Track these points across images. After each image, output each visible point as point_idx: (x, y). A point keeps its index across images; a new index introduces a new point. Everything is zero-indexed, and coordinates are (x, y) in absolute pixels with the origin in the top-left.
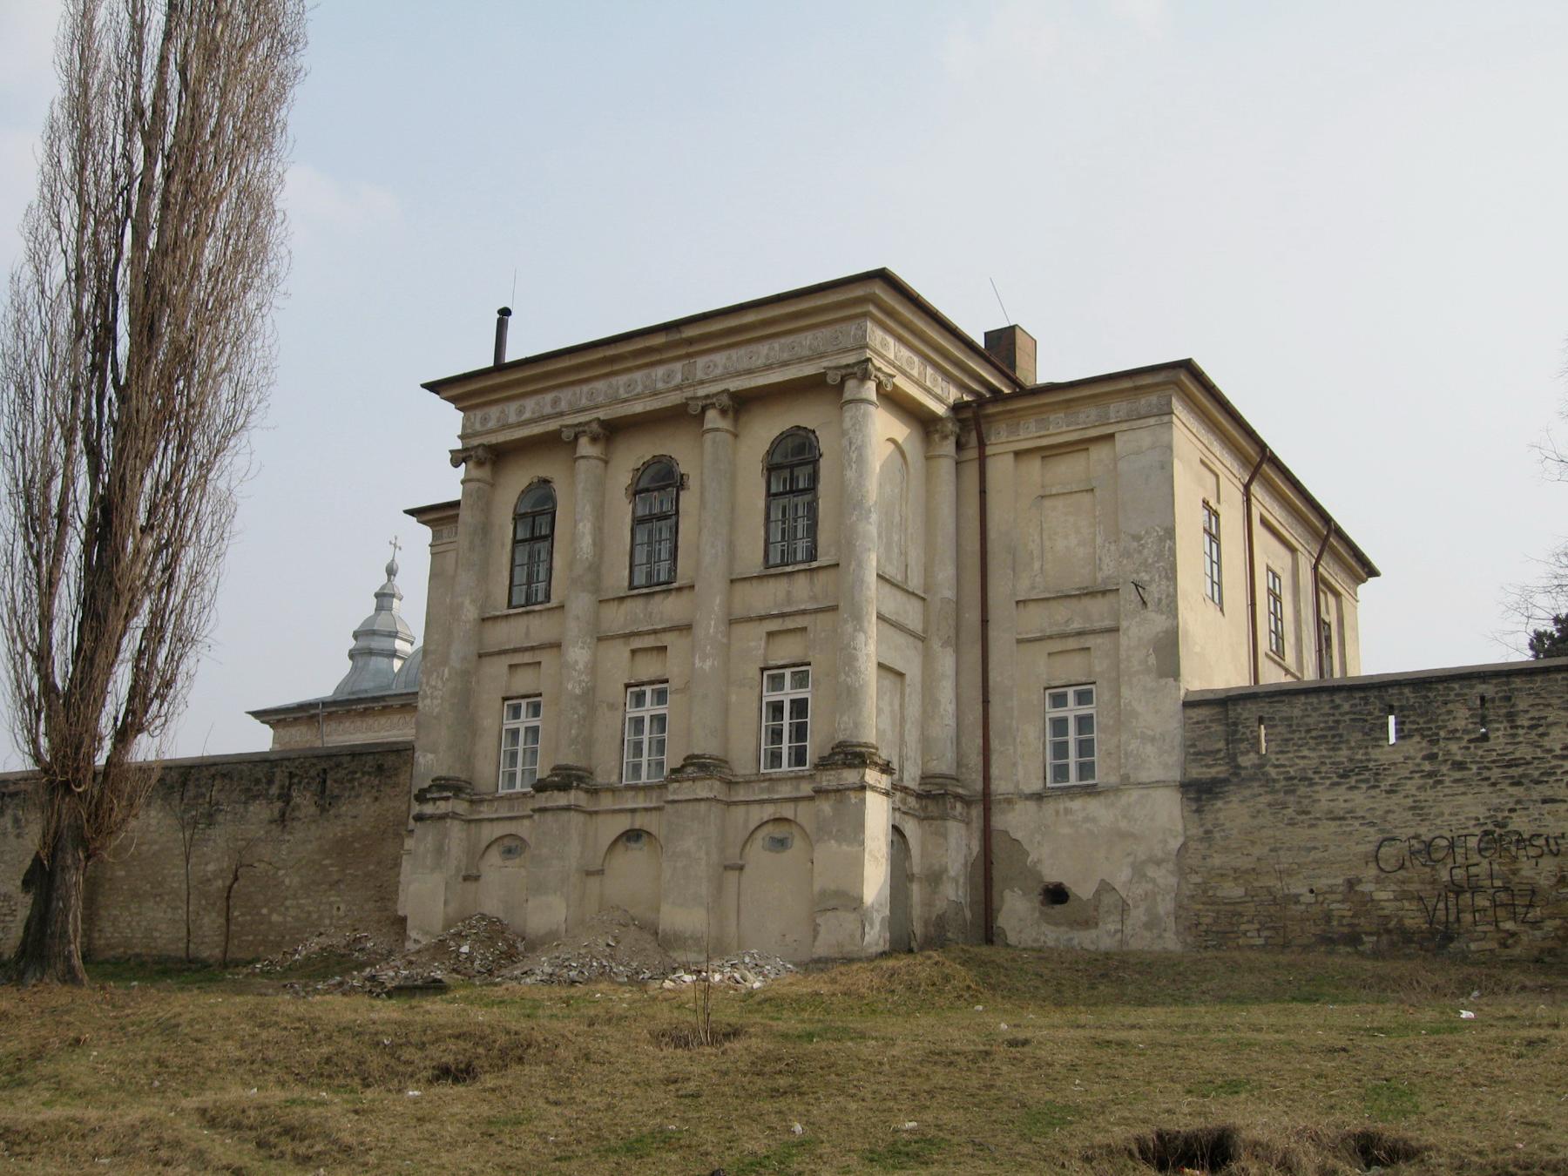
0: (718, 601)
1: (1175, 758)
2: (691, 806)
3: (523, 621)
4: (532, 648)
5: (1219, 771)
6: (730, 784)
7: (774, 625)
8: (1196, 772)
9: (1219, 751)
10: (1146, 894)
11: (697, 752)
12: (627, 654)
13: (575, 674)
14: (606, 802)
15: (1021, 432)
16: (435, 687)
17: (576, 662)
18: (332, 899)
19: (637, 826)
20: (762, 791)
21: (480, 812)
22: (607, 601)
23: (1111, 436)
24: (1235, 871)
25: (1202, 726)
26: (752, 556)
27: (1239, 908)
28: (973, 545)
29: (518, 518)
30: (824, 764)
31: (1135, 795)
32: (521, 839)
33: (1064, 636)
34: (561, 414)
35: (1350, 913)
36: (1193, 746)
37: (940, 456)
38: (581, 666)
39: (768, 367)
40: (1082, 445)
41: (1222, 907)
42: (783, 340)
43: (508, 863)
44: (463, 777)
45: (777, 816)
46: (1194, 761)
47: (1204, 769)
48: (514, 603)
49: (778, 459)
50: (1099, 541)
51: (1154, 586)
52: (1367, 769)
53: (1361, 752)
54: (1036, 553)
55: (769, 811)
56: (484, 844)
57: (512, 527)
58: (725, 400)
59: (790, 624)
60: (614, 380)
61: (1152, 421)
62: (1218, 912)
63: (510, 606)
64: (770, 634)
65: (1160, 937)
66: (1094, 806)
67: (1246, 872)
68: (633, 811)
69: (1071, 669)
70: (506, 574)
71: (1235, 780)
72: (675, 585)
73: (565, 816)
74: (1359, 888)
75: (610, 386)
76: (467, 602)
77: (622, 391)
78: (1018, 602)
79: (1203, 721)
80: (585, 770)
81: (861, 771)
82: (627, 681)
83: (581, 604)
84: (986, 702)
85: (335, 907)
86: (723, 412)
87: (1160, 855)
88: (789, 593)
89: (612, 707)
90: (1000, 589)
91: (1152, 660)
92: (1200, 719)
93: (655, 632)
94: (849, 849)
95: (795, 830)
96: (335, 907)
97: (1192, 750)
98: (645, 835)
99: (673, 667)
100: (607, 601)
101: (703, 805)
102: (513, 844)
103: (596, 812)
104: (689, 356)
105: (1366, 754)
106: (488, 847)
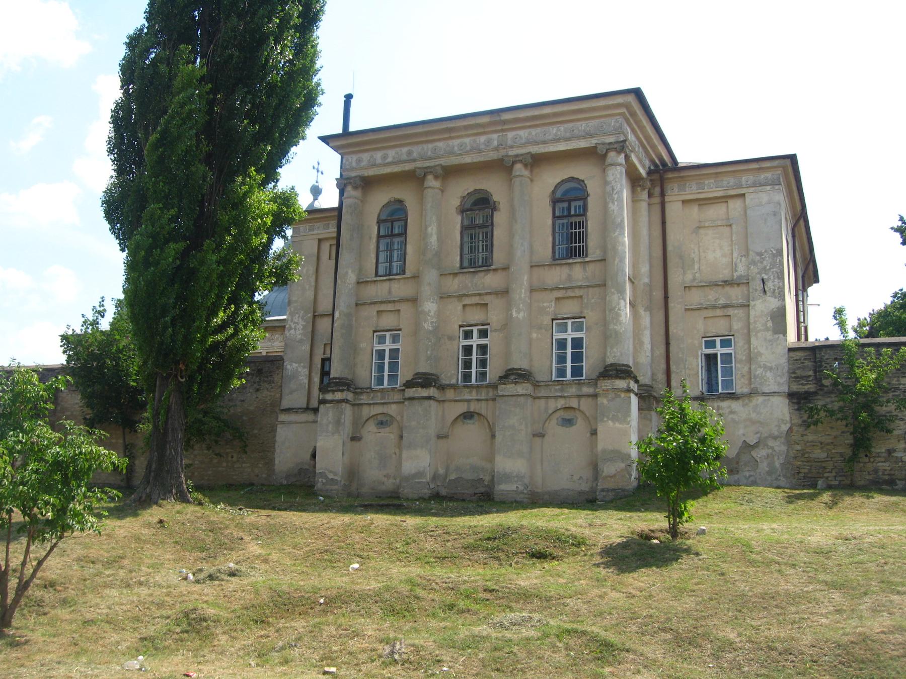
0: (526, 278)
1: (784, 380)
2: (514, 399)
3: (387, 285)
4: (394, 301)
5: (811, 387)
6: (536, 385)
7: (560, 294)
8: (795, 388)
9: (810, 376)
10: (768, 455)
11: (515, 367)
12: (460, 308)
13: (429, 318)
14: (450, 394)
15: (687, 189)
16: (297, 323)
17: (430, 311)
18: (228, 451)
19: (472, 410)
20: (556, 391)
21: (361, 399)
22: (445, 275)
23: (743, 195)
24: (821, 444)
25: (799, 362)
26: (544, 250)
27: (824, 464)
28: (658, 252)
29: (380, 222)
30: (409, 384)
31: (761, 399)
32: (391, 416)
33: (714, 307)
34: (415, 160)
35: (889, 468)
36: (794, 373)
37: (641, 200)
38: (432, 313)
39: (557, 140)
40: (725, 199)
41: (814, 463)
42: (566, 125)
43: (380, 430)
44: (350, 377)
45: (567, 406)
46: (795, 381)
47: (801, 386)
48: (380, 273)
49: (383, 217)
50: (735, 255)
51: (771, 281)
52: (899, 389)
53: (895, 379)
54: (696, 259)
55: (561, 403)
56: (365, 419)
57: (376, 228)
58: (440, 171)
59: (570, 293)
60: (451, 142)
61: (768, 188)
62: (811, 466)
63: (377, 275)
64: (557, 299)
65: (776, 479)
66: (735, 405)
67: (828, 444)
68: (469, 401)
69: (719, 326)
70: (373, 256)
71: (821, 393)
72: (493, 267)
73: (426, 403)
74: (895, 454)
75: (372, 157)
76: (350, 271)
77: (456, 148)
78: (685, 287)
79: (800, 359)
80: (527, 371)
81: (627, 381)
82: (460, 323)
83: (430, 276)
84: (668, 344)
85: (230, 455)
86: (526, 166)
87: (776, 433)
88: (569, 275)
89: (451, 338)
90: (676, 278)
91: (770, 324)
92: (798, 358)
93: (480, 295)
94: (621, 426)
95: (578, 414)
96: (230, 455)
97: (793, 375)
98: (476, 415)
99: (495, 316)
100: (445, 275)
101: (522, 399)
102: (384, 419)
103: (443, 401)
104: (503, 130)
105: (898, 381)
106: (367, 420)
